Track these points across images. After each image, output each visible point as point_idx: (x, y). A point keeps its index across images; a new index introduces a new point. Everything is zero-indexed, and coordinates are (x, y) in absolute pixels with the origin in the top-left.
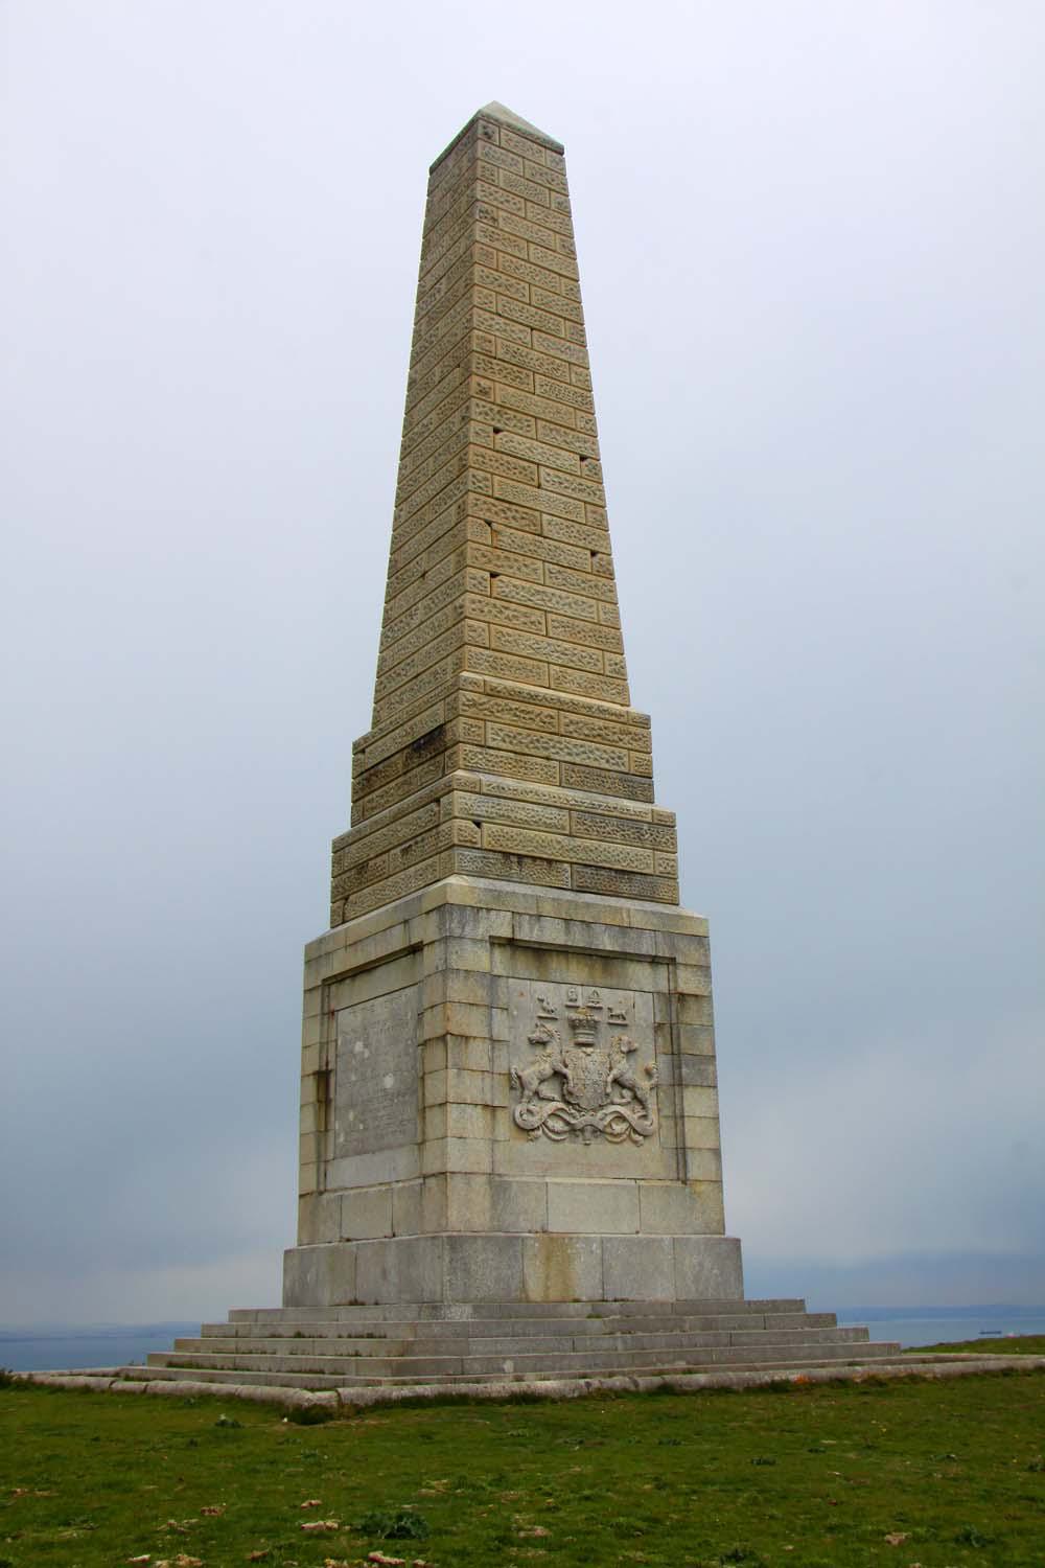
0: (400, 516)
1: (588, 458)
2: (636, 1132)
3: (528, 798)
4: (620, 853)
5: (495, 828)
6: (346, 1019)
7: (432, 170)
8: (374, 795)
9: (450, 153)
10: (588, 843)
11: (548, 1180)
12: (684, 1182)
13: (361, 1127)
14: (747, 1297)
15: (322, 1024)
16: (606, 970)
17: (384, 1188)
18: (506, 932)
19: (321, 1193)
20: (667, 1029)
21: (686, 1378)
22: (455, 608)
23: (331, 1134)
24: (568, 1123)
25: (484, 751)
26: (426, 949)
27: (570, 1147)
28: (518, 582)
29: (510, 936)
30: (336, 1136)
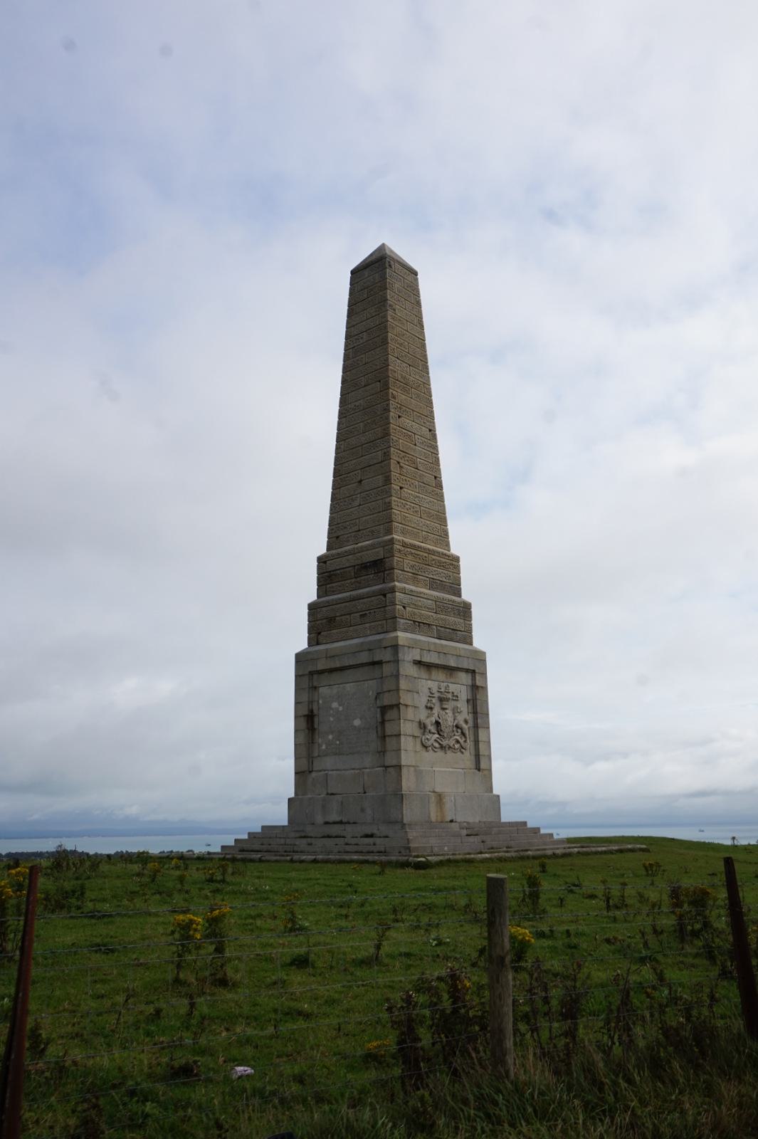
0: (340, 448)
1: (432, 431)
2: (463, 748)
3: (422, 595)
4: (452, 620)
5: (410, 609)
6: (324, 691)
7: (353, 272)
8: (333, 585)
9: (367, 267)
10: (442, 616)
11: (434, 769)
12: (479, 770)
13: (338, 742)
14: (504, 819)
15: (309, 693)
16: (451, 675)
17: (357, 771)
18: (418, 658)
19: (310, 772)
20: (471, 701)
21: (507, 854)
22: (385, 503)
23: (316, 745)
24: (440, 744)
25: (403, 572)
26: (384, 664)
27: (440, 754)
28: (410, 492)
29: (419, 659)
30: (320, 746)
